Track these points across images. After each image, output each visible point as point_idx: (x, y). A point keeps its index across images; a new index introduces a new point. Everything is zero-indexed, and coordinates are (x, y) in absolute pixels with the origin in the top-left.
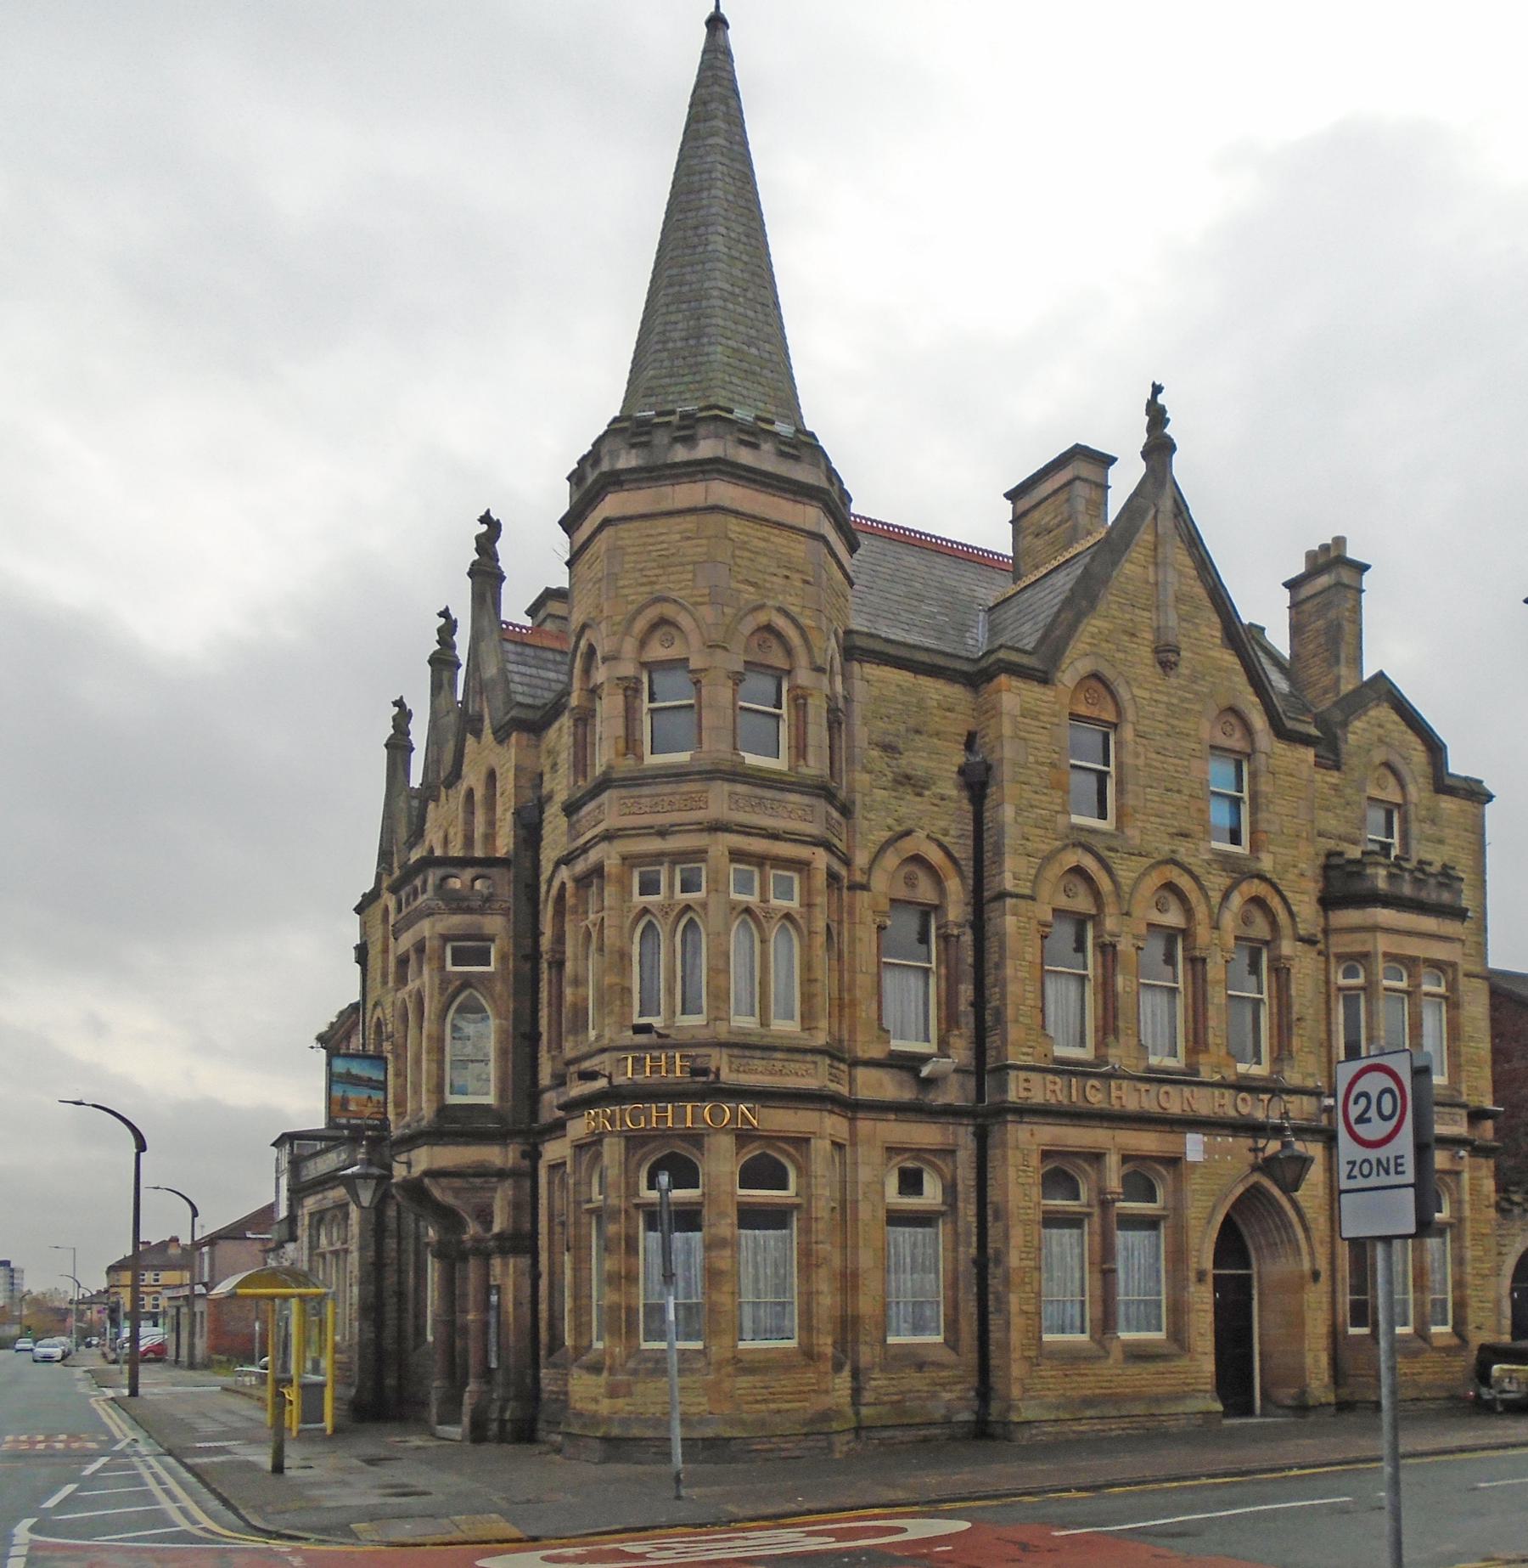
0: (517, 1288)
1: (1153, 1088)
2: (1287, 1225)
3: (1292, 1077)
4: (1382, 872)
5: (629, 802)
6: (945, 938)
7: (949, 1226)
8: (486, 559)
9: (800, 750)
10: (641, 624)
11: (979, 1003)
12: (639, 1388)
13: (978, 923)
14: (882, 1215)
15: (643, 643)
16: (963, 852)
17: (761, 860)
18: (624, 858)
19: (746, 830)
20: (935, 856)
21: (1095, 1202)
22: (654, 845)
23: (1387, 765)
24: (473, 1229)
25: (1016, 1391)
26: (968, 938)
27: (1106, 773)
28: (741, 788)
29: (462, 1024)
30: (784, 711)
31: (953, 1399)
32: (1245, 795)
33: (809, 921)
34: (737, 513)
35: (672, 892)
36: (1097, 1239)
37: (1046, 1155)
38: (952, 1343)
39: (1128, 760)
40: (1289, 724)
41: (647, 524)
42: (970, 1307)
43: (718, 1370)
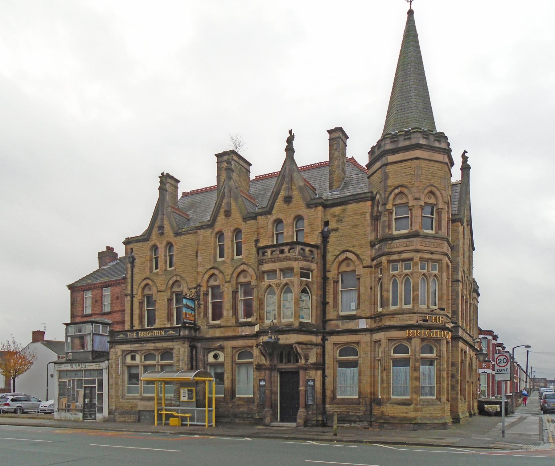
9: (439, 227)
12: (424, 409)
17: (427, 260)
24: (302, 362)
30: (434, 216)
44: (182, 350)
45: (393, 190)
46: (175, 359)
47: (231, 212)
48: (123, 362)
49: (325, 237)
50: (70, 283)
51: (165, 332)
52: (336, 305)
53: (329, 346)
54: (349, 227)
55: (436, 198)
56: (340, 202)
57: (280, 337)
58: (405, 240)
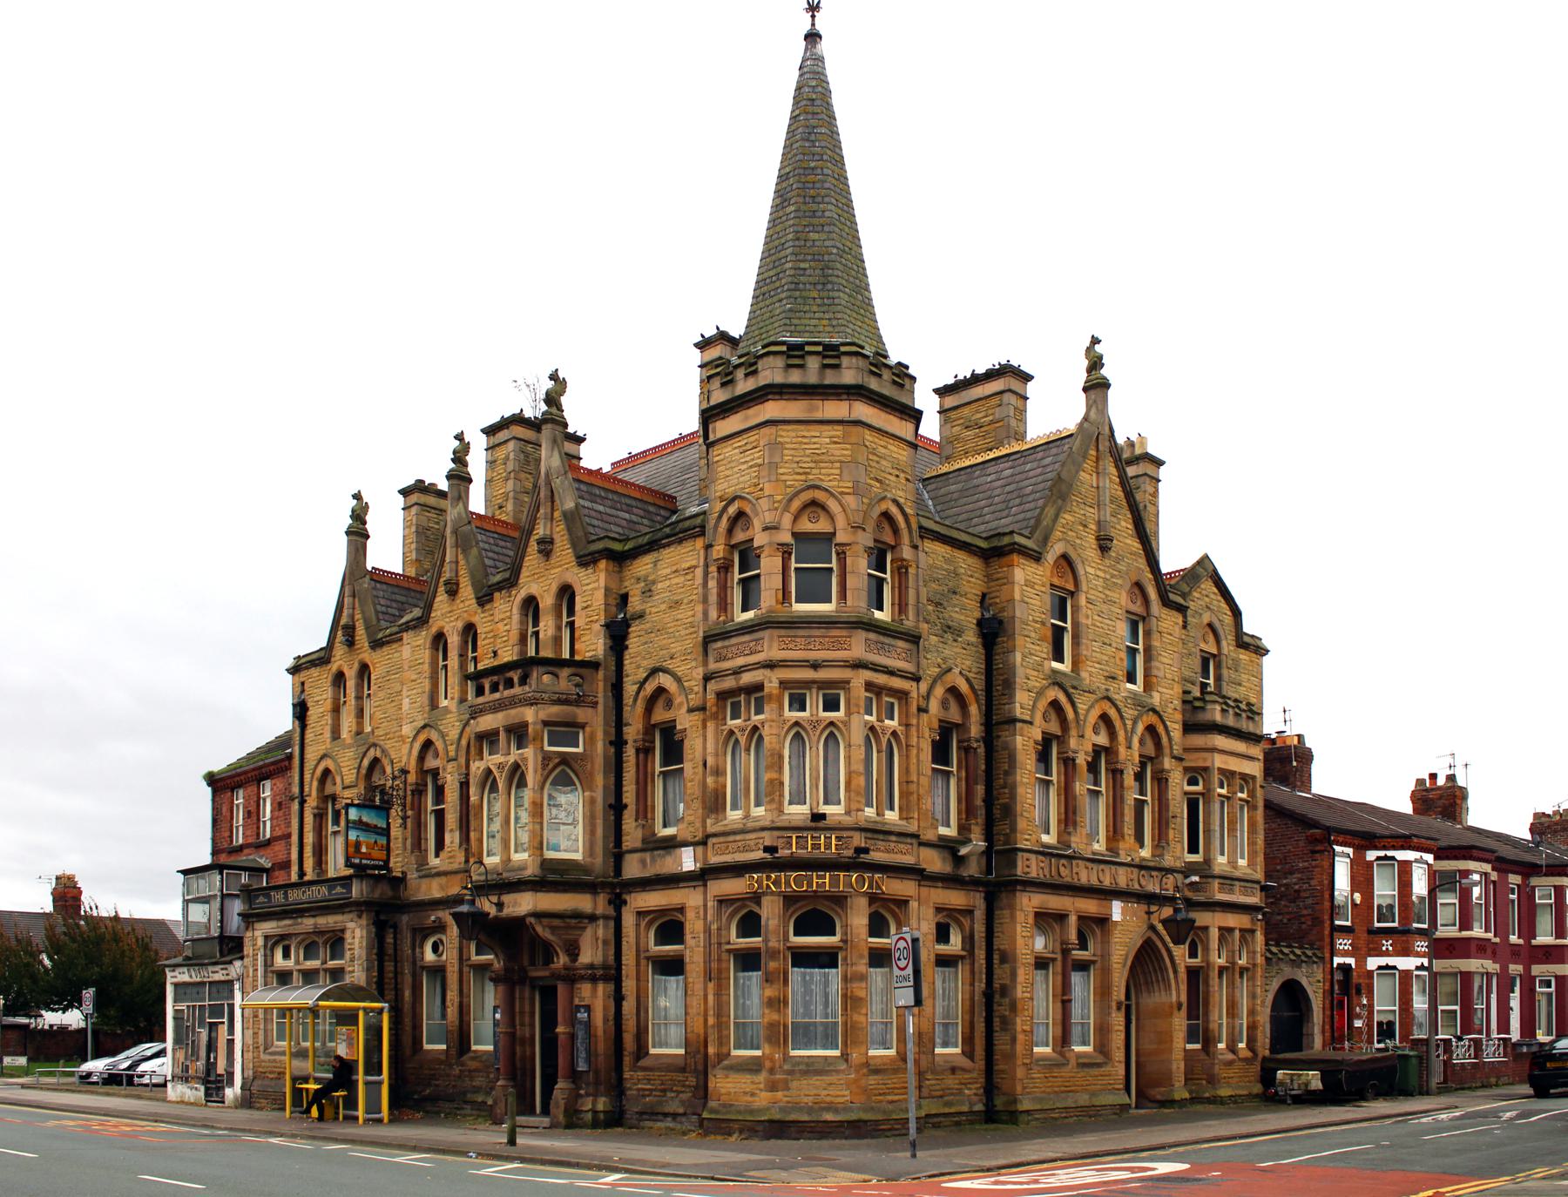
0: (605, 1008)
1: (1095, 866)
2: (1163, 969)
3: (1168, 861)
4: (1218, 708)
5: (787, 640)
6: (966, 750)
7: (967, 967)
8: (554, 410)
10: (796, 504)
11: (989, 800)
12: (794, 1084)
13: (989, 739)
14: (933, 958)
15: (796, 518)
16: (980, 685)
18: (781, 683)
19: (875, 668)
20: (964, 687)
21: (1058, 949)
22: (809, 674)
23: (1210, 625)
24: (562, 960)
25: (1019, 1089)
26: (981, 751)
27: (1064, 629)
28: (872, 636)
29: (555, 794)
31: (971, 1097)
32: (1140, 647)
33: (907, 736)
34: (869, 427)
35: (813, 709)
36: (1059, 978)
37: (939, 910)
38: (968, 1053)
39: (1083, 620)
40: (1172, 596)
41: (802, 427)
42: (980, 1027)
43: (857, 1071)
44: (358, 933)
45: (725, 509)
46: (348, 954)
47: (457, 584)
48: (268, 963)
49: (618, 634)
50: (218, 765)
51: (330, 889)
52: (644, 811)
53: (628, 920)
54: (663, 607)
55: (832, 518)
56: (634, 549)
57: (506, 898)
58: (746, 638)
